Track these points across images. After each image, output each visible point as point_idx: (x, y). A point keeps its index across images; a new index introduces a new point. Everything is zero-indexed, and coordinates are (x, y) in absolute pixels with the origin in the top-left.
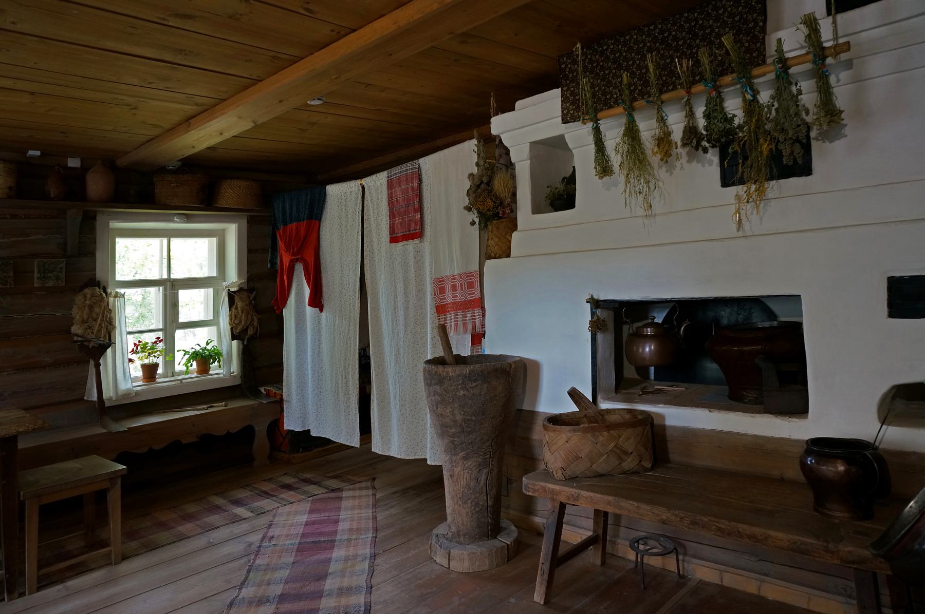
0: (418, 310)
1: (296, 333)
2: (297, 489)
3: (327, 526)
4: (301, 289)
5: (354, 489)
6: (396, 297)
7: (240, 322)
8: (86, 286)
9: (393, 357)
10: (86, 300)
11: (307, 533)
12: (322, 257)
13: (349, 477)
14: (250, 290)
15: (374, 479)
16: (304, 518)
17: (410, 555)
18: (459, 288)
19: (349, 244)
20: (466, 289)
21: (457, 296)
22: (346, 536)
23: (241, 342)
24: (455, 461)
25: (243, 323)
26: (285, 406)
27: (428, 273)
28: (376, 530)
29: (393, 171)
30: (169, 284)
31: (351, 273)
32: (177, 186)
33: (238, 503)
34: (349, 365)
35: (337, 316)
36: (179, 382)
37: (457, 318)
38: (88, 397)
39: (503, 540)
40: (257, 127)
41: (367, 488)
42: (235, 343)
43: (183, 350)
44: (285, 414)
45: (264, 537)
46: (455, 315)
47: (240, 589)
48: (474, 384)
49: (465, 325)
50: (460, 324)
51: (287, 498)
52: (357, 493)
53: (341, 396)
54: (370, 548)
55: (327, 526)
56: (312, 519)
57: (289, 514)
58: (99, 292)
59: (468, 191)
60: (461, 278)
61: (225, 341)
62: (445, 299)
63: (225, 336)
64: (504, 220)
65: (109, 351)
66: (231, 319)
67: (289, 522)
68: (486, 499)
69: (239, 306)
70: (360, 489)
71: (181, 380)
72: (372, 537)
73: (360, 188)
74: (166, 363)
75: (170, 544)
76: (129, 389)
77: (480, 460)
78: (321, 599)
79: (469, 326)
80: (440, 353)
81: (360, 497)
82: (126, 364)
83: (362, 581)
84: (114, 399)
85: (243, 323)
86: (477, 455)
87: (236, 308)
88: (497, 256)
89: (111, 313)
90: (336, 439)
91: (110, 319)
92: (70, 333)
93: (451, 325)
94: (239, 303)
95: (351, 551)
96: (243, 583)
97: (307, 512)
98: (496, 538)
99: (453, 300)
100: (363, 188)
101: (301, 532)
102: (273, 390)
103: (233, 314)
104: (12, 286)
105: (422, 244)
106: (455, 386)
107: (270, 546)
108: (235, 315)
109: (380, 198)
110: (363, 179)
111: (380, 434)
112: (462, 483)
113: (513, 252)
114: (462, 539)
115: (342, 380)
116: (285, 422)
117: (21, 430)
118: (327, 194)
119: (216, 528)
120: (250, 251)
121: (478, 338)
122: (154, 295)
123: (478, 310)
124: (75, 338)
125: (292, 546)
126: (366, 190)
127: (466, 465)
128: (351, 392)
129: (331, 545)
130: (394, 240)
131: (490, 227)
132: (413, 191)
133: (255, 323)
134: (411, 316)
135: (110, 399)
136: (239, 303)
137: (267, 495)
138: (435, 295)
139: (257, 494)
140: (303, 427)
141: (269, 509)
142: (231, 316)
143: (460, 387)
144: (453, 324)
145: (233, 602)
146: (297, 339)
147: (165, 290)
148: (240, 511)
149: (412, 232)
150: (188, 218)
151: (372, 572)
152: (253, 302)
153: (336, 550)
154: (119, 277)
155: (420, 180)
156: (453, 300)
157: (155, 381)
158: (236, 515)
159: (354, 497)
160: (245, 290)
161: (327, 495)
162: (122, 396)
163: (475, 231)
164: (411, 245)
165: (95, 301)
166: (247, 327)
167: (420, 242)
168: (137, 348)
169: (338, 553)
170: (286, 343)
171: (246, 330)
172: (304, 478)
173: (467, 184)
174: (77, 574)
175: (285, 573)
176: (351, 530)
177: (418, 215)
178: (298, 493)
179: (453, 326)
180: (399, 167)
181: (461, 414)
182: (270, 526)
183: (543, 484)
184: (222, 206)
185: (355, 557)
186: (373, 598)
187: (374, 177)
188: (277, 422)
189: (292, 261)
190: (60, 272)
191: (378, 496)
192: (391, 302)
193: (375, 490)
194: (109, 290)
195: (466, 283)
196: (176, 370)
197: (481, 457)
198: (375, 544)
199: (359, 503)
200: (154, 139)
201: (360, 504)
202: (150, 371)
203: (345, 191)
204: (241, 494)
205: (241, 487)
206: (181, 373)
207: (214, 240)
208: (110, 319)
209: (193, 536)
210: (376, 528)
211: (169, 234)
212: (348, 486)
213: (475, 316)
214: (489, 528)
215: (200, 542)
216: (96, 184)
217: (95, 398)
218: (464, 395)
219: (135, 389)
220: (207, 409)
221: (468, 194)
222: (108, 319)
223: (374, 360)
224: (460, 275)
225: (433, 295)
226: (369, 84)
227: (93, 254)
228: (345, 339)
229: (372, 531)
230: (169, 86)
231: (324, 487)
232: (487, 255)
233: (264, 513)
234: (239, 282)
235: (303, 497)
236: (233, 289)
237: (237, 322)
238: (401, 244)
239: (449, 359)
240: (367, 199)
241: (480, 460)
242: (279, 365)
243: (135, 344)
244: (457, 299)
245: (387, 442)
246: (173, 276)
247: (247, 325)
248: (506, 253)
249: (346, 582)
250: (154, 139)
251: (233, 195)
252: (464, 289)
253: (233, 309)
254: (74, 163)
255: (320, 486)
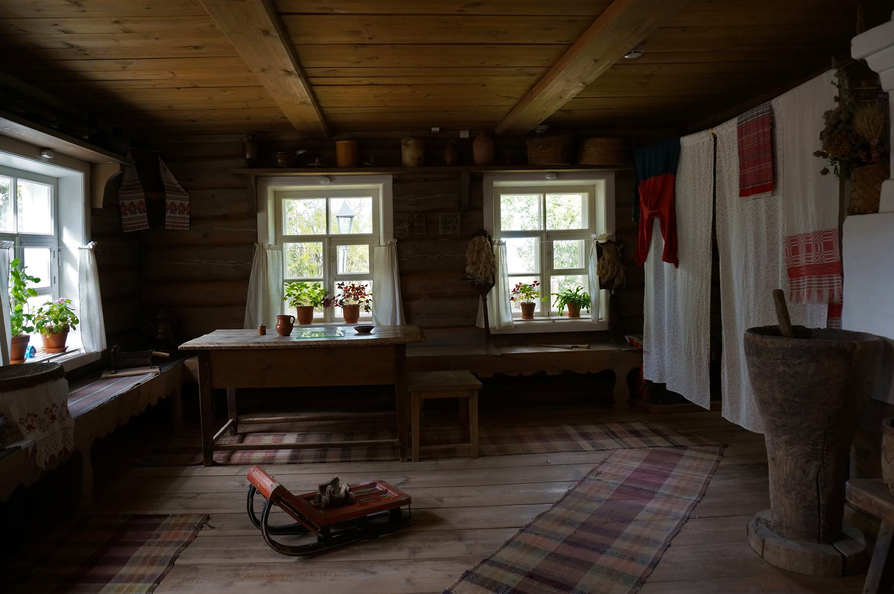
0: (769, 271)
1: (655, 286)
2: (643, 436)
3: (655, 477)
4: (657, 243)
5: (700, 451)
6: (746, 255)
7: (607, 273)
8: (476, 234)
9: (744, 321)
10: (475, 246)
11: (633, 478)
12: (677, 212)
13: (700, 438)
14: (618, 243)
15: (726, 446)
16: (636, 465)
17: (725, 530)
18: (813, 248)
19: (702, 198)
20: (823, 250)
21: (811, 259)
22: (669, 492)
23: (609, 291)
24: (777, 444)
25: (609, 273)
26: (644, 357)
27: (781, 231)
28: (703, 495)
29: (744, 116)
30: (544, 235)
31: (704, 229)
32: (544, 147)
33: (585, 436)
34: (701, 323)
35: (691, 273)
36: (552, 321)
37: (811, 284)
38: (479, 325)
39: (840, 550)
40: (588, 87)
41: (714, 453)
42: (603, 291)
43: (557, 294)
44: (644, 365)
45: (592, 471)
46: (808, 281)
47: (553, 507)
48: (798, 361)
49: (820, 292)
50: (815, 291)
51: (630, 443)
52: (701, 455)
53: (693, 354)
54: (687, 510)
55: (655, 477)
56: (654, 469)
57: (624, 457)
58: (485, 240)
59: (821, 133)
60: (816, 237)
61: (593, 289)
62: (798, 260)
63: (594, 284)
64: (870, 166)
65: (494, 288)
66: (598, 269)
67: (621, 464)
68: (816, 495)
69: (606, 257)
70: (706, 452)
71: (554, 320)
72: (695, 501)
73: (712, 137)
74: (542, 304)
75: (518, 454)
76: (510, 322)
77: (808, 449)
78: (616, 539)
79: (826, 294)
80: (773, 321)
81: (702, 459)
82: (508, 301)
83: (663, 537)
84: (497, 329)
85: (609, 273)
86: (804, 443)
87: (604, 259)
88: (862, 210)
89: (494, 258)
90: (688, 397)
91: (493, 262)
92: (465, 272)
93: (804, 292)
94: (606, 255)
95: (666, 507)
96: (558, 503)
97: (642, 460)
98: (831, 544)
99: (807, 262)
100: (715, 138)
101: (627, 476)
102: (636, 340)
103: (601, 265)
104: (425, 234)
105: (775, 197)
106: (774, 359)
107: (594, 480)
108: (602, 265)
109: (731, 147)
110: (715, 128)
111: (729, 400)
112: (785, 469)
113: (883, 206)
114: (784, 531)
115: (694, 338)
116: (644, 372)
117: (406, 341)
118: (682, 146)
119: (558, 452)
120: (618, 205)
121: (835, 310)
122: (533, 243)
123: (837, 276)
124: (468, 277)
125: (613, 485)
126: (718, 139)
127: (790, 451)
128: (702, 352)
129: (651, 495)
130: (744, 193)
131: (852, 175)
132: (764, 138)
133: (622, 275)
134: (762, 277)
135: (494, 329)
136: (606, 255)
137: (614, 435)
138: (787, 255)
139: (605, 432)
140: (661, 379)
141: (609, 448)
142: (598, 266)
143: (779, 361)
144: (805, 290)
145: (543, 515)
146: (656, 292)
147: (541, 240)
148: (584, 443)
149: (763, 184)
150: (559, 176)
151: (677, 532)
152: (620, 254)
153: (653, 501)
154: (504, 228)
155: (773, 125)
156: (807, 262)
157: (532, 318)
158: (579, 446)
159: (695, 458)
160: (613, 243)
161: (668, 449)
162: (504, 327)
163: (833, 182)
164: (762, 200)
165: (481, 247)
166: (614, 278)
167: (772, 195)
168: (518, 289)
169: (653, 505)
170: (646, 295)
171: (614, 279)
172: (654, 428)
173: (821, 125)
174: (447, 457)
175: (596, 506)
176: (676, 488)
177: (769, 164)
178: (642, 441)
179: (805, 292)
180: (750, 112)
181: (780, 392)
182: (603, 462)
183: (869, 495)
184: (586, 163)
185: (668, 513)
186: (666, 556)
187: (725, 125)
188: (637, 371)
189: (650, 215)
190: (456, 223)
191: (722, 463)
192: (741, 262)
193: (721, 457)
194: (493, 239)
195: (822, 243)
196: (552, 311)
197: (809, 446)
198: (694, 508)
199: (697, 465)
200: (513, 109)
201: (698, 466)
202: (528, 309)
203: (698, 142)
204: (591, 429)
205: (595, 423)
206: (555, 314)
207: (586, 195)
208: (493, 262)
209: (537, 453)
210: (704, 493)
211: (544, 191)
212: (695, 446)
213: (833, 283)
214: (821, 530)
215: (540, 459)
216: (480, 152)
217: (484, 327)
218: (785, 371)
219: (515, 323)
220: (571, 349)
221: (822, 137)
222: (492, 263)
223: (725, 323)
224: (816, 233)
225: (785, 255)
226: (685, 28)
227: (481, 209)
228: (698, 297)
229: (698, 495)
230: (498, 63)
231: (670, 442)
232: (848, 209)
233: (603, 450)
234: (607, 235)
235: (645, 445)
236: (601, 242)
237: (604, 272)
238: (751, 197)
239: (784, 329)
240: (719, 149)
241: (808, 449)
242: (641, 317)
243: (517, 286)
244: (811, 262)
245: (736, 410)
246: (548, 228)
247: (614, 275)
248: (874, 208)
249: (647, 532)
250: (513, 109)
251: (594, 152)
252: (819, 250)
253: (601, 260)
254: (464, 135)
255: (666, 439)
